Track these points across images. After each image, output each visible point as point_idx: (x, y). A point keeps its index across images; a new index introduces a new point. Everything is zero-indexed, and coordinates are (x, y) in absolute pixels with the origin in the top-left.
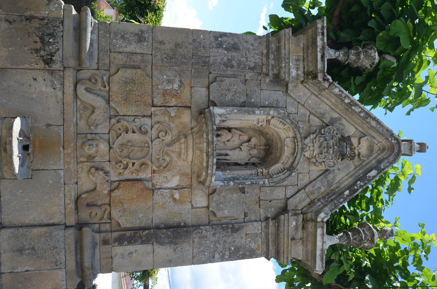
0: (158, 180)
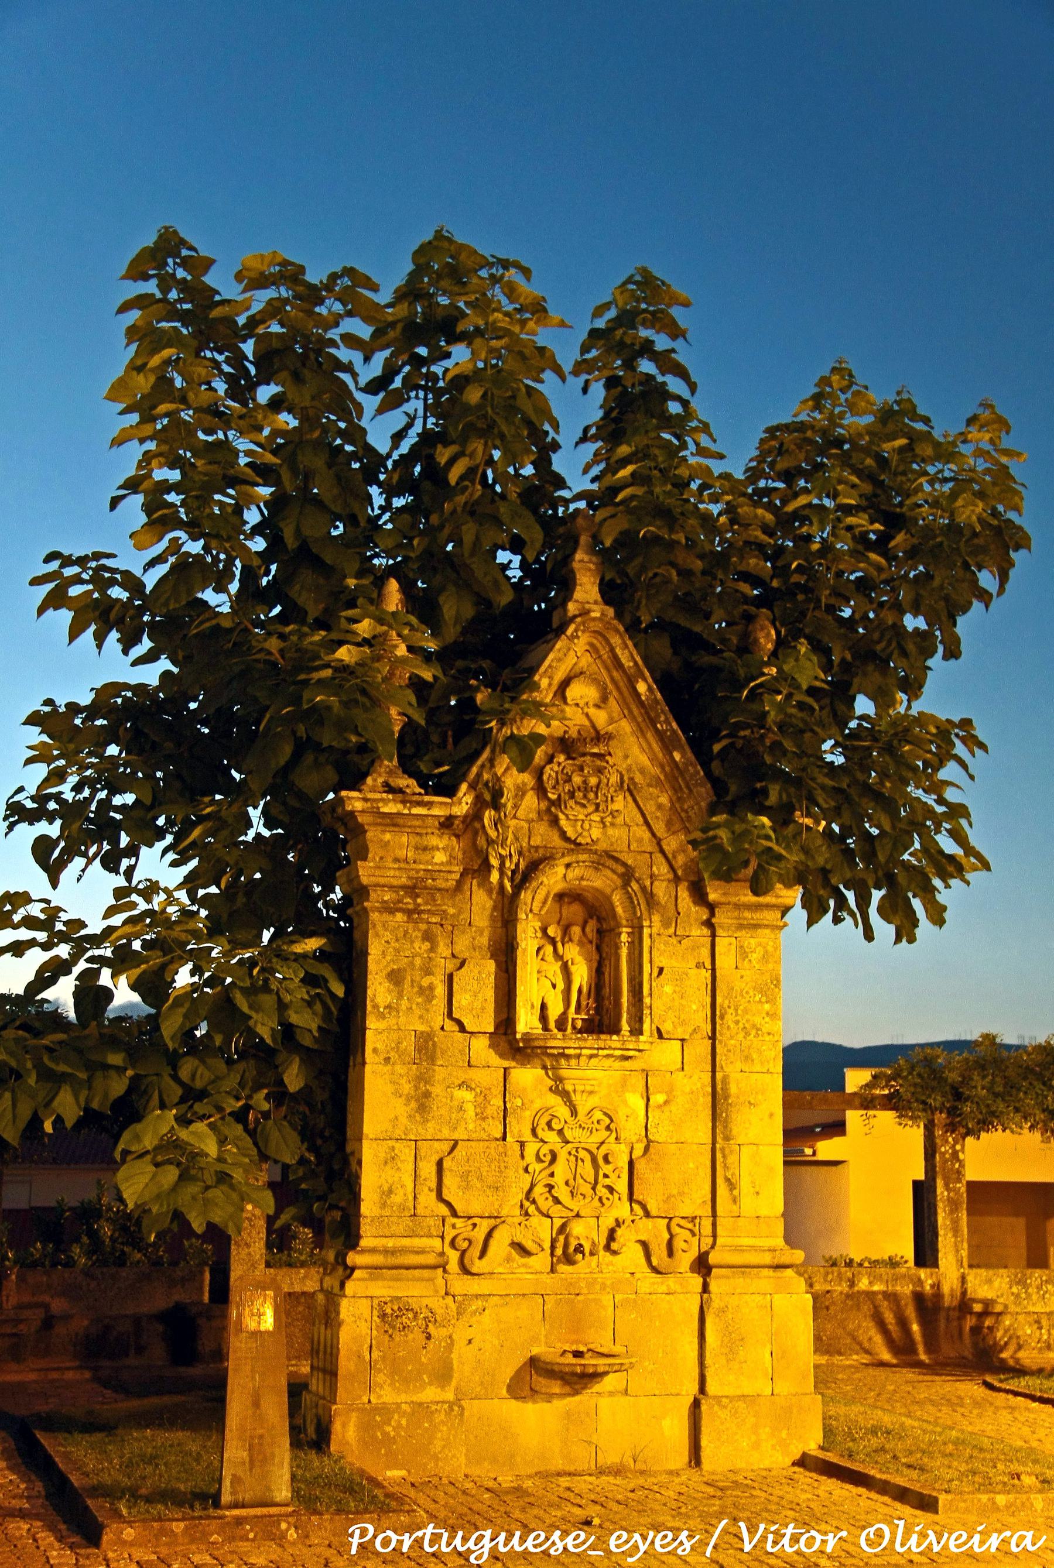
0: (631, 1129)
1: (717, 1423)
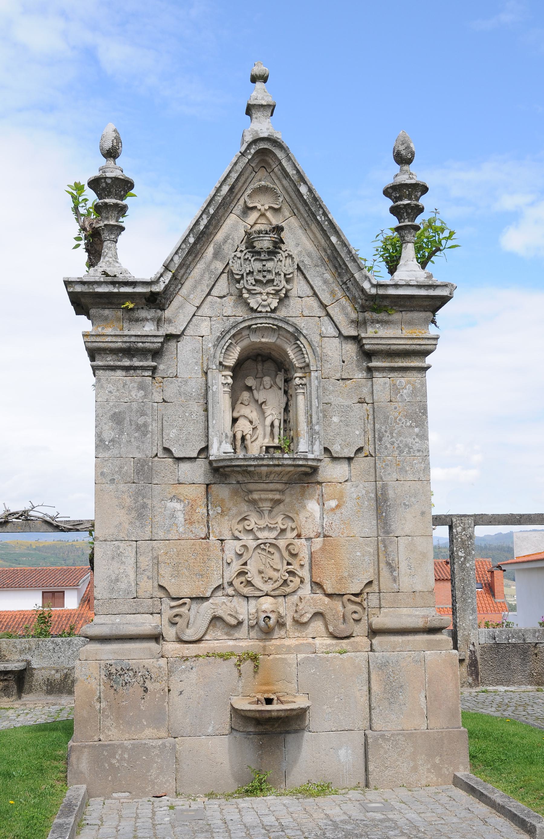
1: (382, 752)
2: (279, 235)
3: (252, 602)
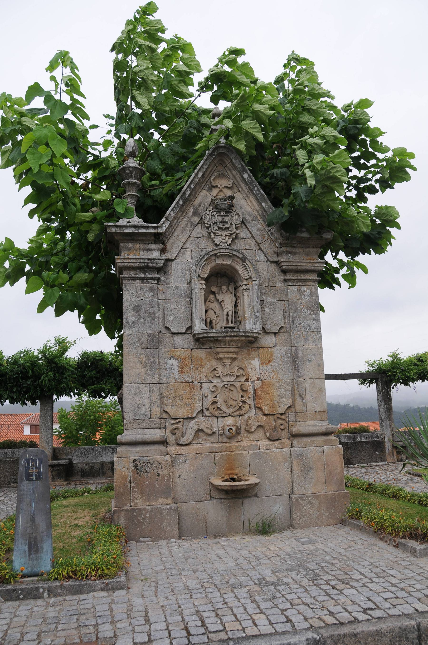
2: (232, 201)
3: (220, 420)
